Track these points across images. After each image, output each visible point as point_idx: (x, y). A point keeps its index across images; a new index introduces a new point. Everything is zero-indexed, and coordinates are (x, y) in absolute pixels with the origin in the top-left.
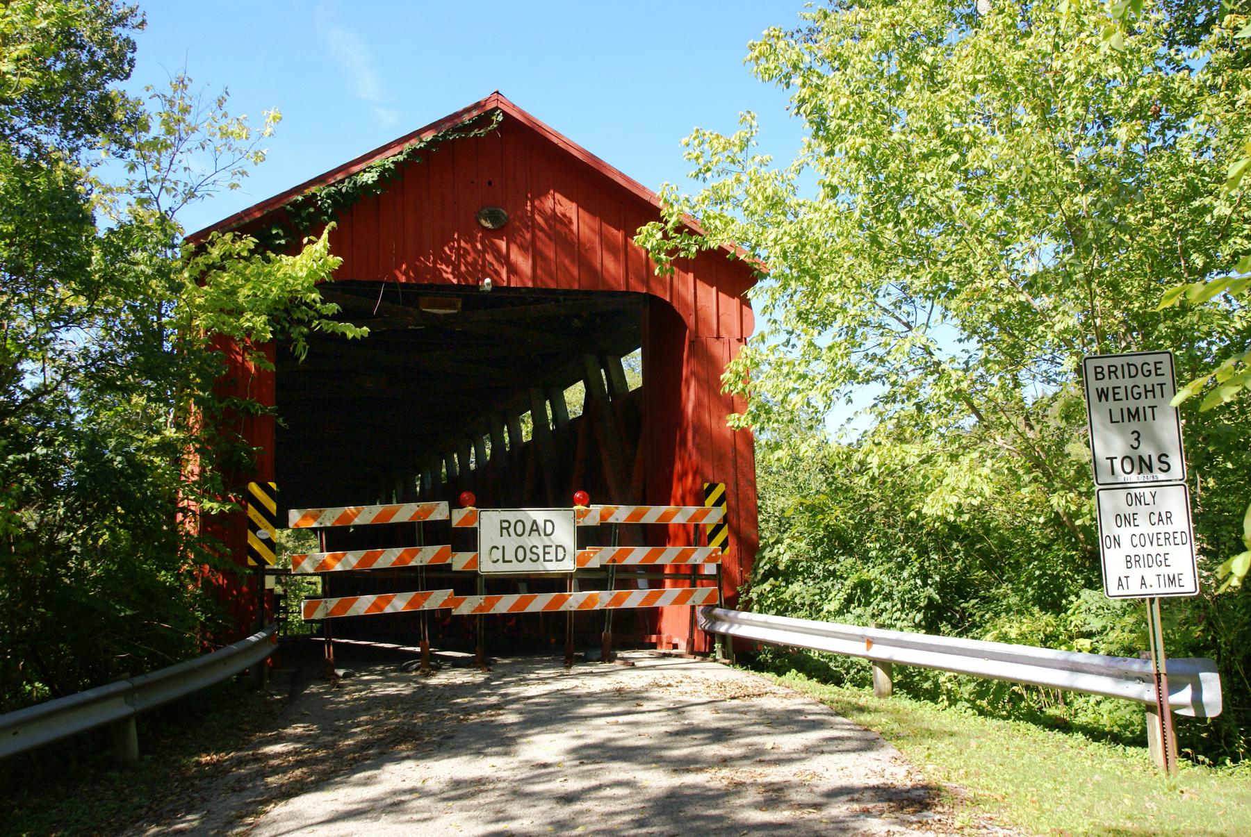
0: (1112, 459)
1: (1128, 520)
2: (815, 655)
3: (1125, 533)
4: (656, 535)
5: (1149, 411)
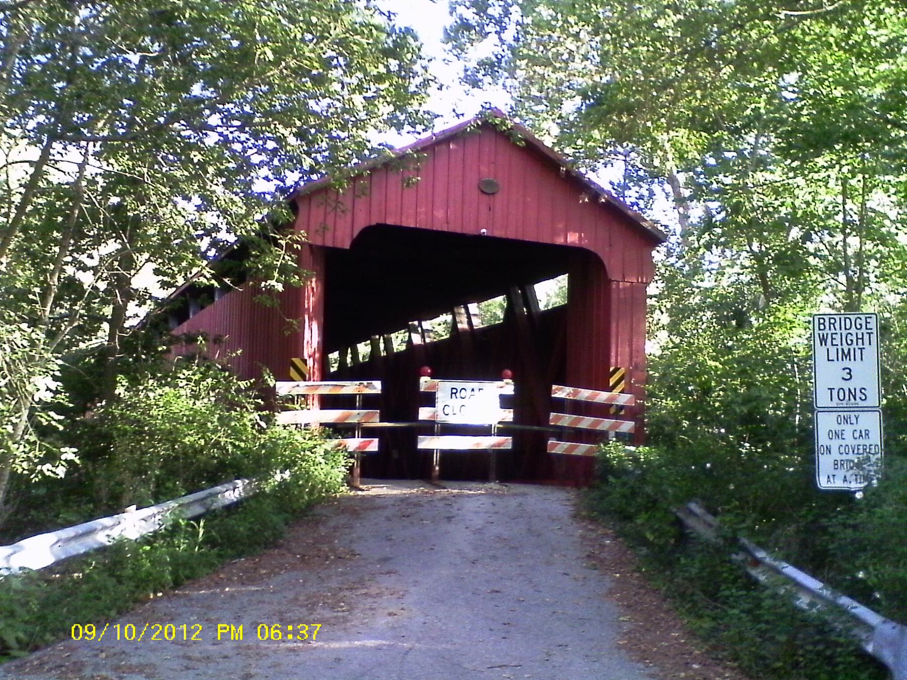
0: (831, 389)
1: (838, 435)
2: (16, 584)
3: (835, 444)
4: (602, 410)
5: (858, 352)
